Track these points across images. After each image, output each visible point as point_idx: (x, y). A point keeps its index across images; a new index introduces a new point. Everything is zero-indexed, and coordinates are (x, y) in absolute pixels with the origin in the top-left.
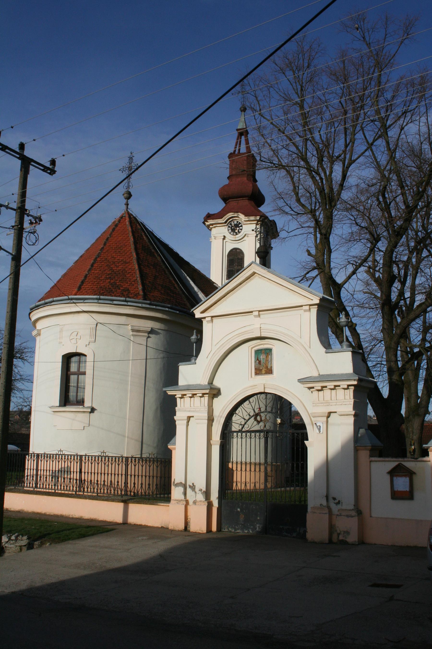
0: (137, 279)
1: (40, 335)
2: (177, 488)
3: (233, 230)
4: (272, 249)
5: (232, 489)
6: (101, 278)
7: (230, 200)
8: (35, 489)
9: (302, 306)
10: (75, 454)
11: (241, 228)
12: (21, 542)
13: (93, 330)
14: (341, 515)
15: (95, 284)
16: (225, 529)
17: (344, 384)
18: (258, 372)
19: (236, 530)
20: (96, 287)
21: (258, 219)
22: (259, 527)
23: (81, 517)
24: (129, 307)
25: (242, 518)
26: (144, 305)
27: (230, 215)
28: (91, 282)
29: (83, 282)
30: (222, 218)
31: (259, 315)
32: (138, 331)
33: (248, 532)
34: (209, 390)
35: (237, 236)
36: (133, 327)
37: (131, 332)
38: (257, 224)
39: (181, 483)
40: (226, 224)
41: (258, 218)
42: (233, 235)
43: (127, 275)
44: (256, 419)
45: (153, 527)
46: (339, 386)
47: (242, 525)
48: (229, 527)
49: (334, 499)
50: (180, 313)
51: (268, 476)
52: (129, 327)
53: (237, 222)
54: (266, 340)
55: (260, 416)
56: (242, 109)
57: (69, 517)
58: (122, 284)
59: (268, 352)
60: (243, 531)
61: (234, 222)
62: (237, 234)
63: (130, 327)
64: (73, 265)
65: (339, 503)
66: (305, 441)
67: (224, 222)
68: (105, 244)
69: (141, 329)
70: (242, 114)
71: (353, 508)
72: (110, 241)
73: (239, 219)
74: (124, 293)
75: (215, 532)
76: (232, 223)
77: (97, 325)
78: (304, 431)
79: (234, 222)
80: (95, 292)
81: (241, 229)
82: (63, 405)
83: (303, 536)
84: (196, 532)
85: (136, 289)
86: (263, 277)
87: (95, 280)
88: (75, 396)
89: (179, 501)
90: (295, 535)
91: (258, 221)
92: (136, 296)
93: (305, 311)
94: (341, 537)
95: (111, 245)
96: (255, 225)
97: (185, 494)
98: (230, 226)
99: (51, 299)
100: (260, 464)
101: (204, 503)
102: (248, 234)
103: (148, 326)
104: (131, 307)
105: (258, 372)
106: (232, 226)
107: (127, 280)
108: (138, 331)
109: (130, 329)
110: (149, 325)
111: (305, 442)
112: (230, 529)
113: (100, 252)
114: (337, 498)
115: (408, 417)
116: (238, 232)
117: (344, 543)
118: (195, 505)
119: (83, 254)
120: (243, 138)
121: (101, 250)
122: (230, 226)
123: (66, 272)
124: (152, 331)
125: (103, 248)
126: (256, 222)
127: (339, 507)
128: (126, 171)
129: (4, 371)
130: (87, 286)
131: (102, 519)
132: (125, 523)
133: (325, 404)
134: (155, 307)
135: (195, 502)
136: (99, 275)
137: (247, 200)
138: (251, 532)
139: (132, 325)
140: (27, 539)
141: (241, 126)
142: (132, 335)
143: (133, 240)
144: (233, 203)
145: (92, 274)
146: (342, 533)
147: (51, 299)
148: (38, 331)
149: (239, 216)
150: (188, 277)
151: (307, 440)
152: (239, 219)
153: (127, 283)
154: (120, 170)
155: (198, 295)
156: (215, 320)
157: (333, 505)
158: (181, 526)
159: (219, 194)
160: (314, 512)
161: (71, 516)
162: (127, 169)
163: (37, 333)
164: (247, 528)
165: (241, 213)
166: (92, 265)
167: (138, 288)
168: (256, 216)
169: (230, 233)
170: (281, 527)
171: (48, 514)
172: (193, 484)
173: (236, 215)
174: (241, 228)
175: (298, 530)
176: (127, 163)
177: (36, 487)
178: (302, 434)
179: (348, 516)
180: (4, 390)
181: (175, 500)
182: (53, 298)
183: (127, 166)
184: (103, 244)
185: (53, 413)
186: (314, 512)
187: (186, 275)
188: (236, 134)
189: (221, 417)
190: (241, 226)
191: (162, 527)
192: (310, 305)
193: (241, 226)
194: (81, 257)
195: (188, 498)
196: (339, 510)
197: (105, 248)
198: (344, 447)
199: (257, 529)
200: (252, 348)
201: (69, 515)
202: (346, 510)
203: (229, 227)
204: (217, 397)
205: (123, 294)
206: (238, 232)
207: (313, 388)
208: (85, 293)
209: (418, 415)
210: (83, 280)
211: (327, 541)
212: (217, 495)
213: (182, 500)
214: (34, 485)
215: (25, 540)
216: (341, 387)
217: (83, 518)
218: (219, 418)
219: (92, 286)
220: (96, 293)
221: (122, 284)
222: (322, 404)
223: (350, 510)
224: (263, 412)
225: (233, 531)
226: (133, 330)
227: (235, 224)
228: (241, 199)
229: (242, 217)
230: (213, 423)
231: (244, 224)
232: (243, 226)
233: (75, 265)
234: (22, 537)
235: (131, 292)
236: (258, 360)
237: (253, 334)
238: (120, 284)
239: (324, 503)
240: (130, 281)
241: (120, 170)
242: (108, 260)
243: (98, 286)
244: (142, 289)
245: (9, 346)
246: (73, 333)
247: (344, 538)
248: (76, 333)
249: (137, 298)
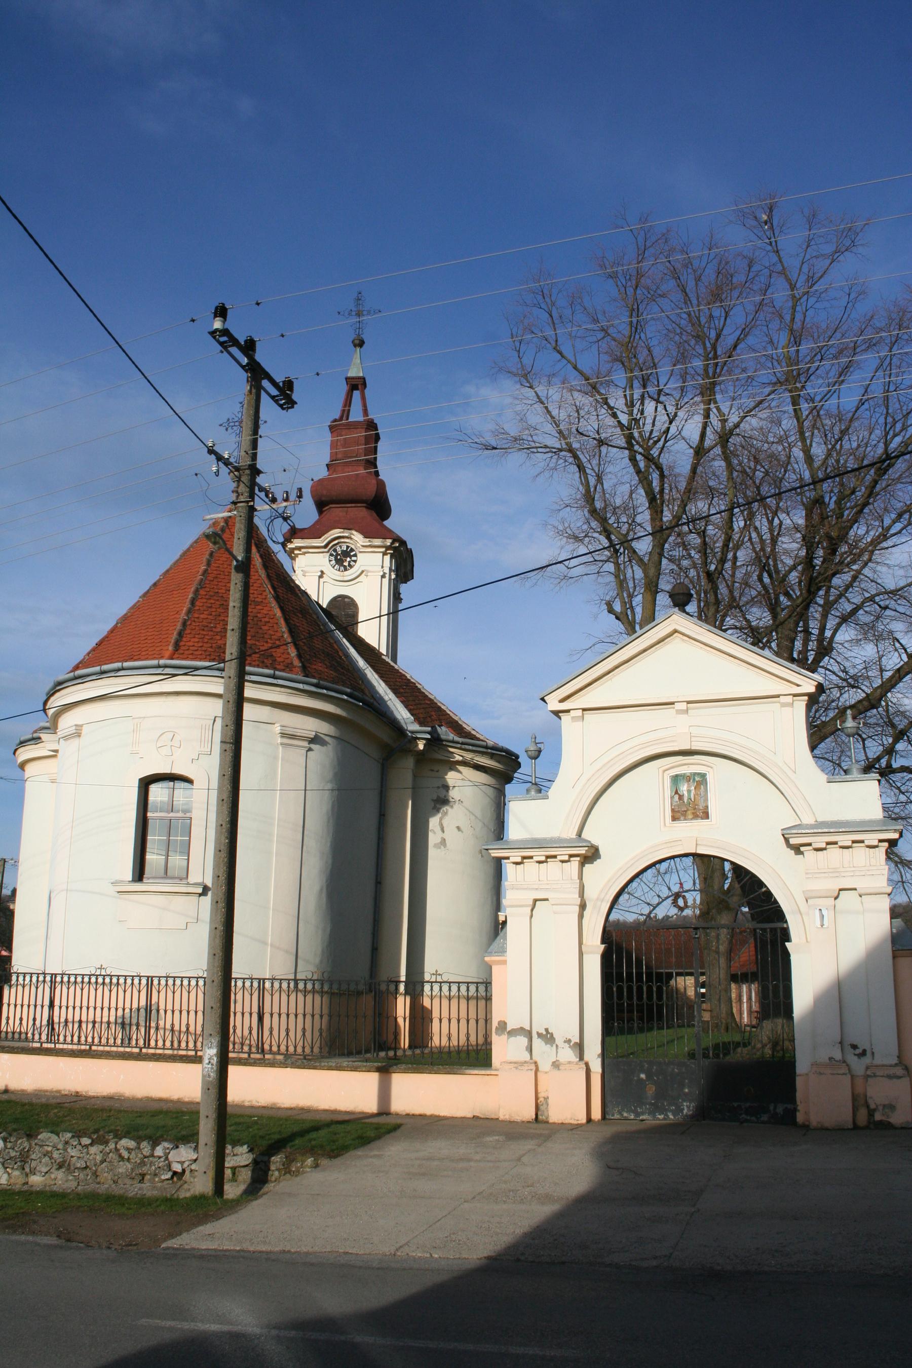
0: (282, 636)
1: (80, 736)
2: (512, 1039)
3: (339, 562)
4: (401, 602)
5: (396, 1048)
6: (214, 629)
7: (331, 506)
8: (144, 1050)
9: (778, 696)
10: (248, 977)
11: (354, 558)
12: (235, 1158)
13: (207, 731)
14: (875, 1076)
15: (206, 641)
16: (613, 1115)
17: (563, 854)
18: (677, 815)
19: (637, 1114)
20: (210, 645)
21: (389, 544)
22: (688, 1107)
23: (274, 1104)
24: (278, 689)
25: (651, 1090)
26: (307, 687)
27: (336, 533)
28: (197, 636)
29: (180, 635)
30: (320, 538)
31: (687, 711)
32: (293, 737)
33: (664, 1119)
34: (586, 848)
35: (346, 573)
36: (284, 728)
37: (279, 739)
38: (384, 554)
39: (522, 1028)
40: (326, 550)
41: (388, 542)
42: (339, 570)
43: (264, 628)
44: (675, 903)
45: (453, 1117)
46: (531, 857)
47: (651, 1104)
48: (623, 1110)
49: (854, 1047)
50: (365, 706)
51: (704, 1010)
52: (277, 729)
53: (348, 547)
54: (696, 757)
55: (684, 897)
56: (357, 342)
57: (244, 1106)
58: (257, 643)
59: (701, 780)
60: (654, 1116)
61: (341, 547)
62: (346, 570)
63: (279, 728)
64: (138, 601)
65: (864, 1053)
66: (786, 943)
67: (323, 545)
68: (209, 564)
69: (299, 733)
70: (356, 351)
71: (897, 1062)
72: (218, 558)
73: (351, 542)
74: (265, 661)
75: (599, 1121)
76: (338, 549)
77: (215, 721)
78: (785, 926)
79: (341, 547)
80: (209, 655)
81: (355, 561)
82: (137, 879)
83: (789, 1118)
84: (562, 1123)
85: (286, 656)
86: (691, 641)
87: (204, 633)
88: (163, 863)
89: (518, 1065)
90: (765, 1118)
91: (388, 548)
92: (289, 667)
93: (784, 705)
94: (878, 1117)
95: (221, 566)
96: (381, 554)
97: (530, 1049)
98: (334, 554)
99: (118, 665)
100: (477, 998)
101: (577, 1066)
102: (368, 571)
103: (309, 728)
104: (282, 689)
105: (677, 815)
106: (337, 554)
107: (266, 636)
108: (293, 737)
109: (279, 732)
110: (310, 726)
111: (787, 944)
112: (625, 1114)
113: (202, 579)
114: (859, 1046)
115: (708, 913)
116: (349, 565)
117: (886, 1126)
118: (559, 1069)
119: (159, 581)
120: (356, 394)
121: (203, 575)
122: (334, 554)
123: (126, 614)
124: (315, 740)
125: (205, 571)
126: (383, 550)
127: (867, 1060)
128: (235, 428)
129: (226, 799)
130: (191, 644)
131: (327, 1107)
132: (384, 1111)
133: (831, 875)
134: (325, 691)
135: (556, 1065)
136: (211, 623)
137: (364, 509)
138: (671, 1117)
139: (284, 723)
140: (249, 1151)
141: (355, 371)
142: (282, 744)
143: (260, 560)
144: (336, 512)
145: (196, 620)
146: (881, 1108)
147: (118, 665)
148: (78, 728)
149: (353, 537)
150: (344, 640)
151: (789, 940)
152: (351, 542)
153: (267, 642)
154: (221, 425)
155: (365, 675)
156: (588, 715)
157: (852, 1059)
158: (530, 1114)
159: (312, 492)
160: (821, 1074)
161: (247, 1104)
162: (237, 424)
163: (74, 731)
164: (663, 1111)
165: (356, 531)
166: (193, 602)
167: (288, 654)
168: (385, 538)
169: (333, 567)
170: (736, 1104)
171: (187, 1100)
172: (547, 1030)
173: (347, 535)
174: (354, 558)
175: (772, 1108)
176: (236, 414)
177: (147, 1045)
178: (774, 930)
179: (889, 1077)
180: (227, 838)
181: (510, 1063)
182: (101, 665)
183: (236, 419)
184: (205, 563)
185: (117, 895)
186: (821, 1074)
187: (341, 636)
188: (345, 388)
189: (602, 901)
190: (355, 555)
191: (474, 1116)
192: (795, 695)
193: (355, 555)
194: (155, 585)
195: (536, 1057)
196: (867, 1068)
197: (209, 572)
198: (872, 955)
199: (685, 1111)
200: (664, 771)
201: (243, 1102)
202: (883, 1066)
203: (331, 555)
204: (592, 863)
205: (263, 662)
206: (349, 565)
207: (531, 857)
208: (190, 656)
209: (728, 908)
210: (181, 630)
211: (850, 1126)
212: (598, 1049)
213: (526, 1062)
214: (141, 1042)
215: (242, 1154)
216: (559, 858)
217: (278, 1105)
218: (599, 903)
219: (200, 644)
220: (213, 657)
221: (257, 643)
222: (826, 875)
223: (891, 1066)
224: (687, 891)
225: (632, 1117)
226: (283, 735)
227: (343, 551)
228: (353, 505)
229: (358, 539)
230: (585, 913)
231: (361, 552)
232: (359, 555)
233: (143, 600)
234: (233, 1148)
235: (278, 659)
236: (676, 792)
237: (675, 744)
238: (254, 642)
239: (838, 1055)
240: (271, 639)
241: (221, 425)
242: (221, 595)
243: (214, 645)
244: (297, 655)
245: (235, 748)
246: (164, 735)
247: (884, 1118)
248: (170, 735)
249: (291, 671)
